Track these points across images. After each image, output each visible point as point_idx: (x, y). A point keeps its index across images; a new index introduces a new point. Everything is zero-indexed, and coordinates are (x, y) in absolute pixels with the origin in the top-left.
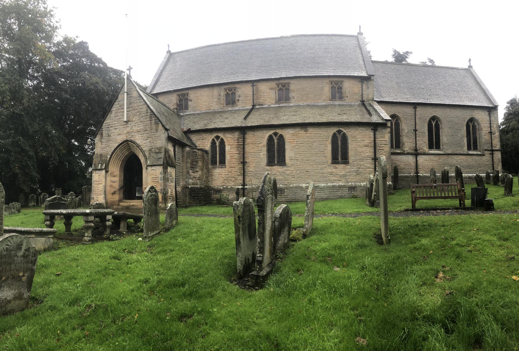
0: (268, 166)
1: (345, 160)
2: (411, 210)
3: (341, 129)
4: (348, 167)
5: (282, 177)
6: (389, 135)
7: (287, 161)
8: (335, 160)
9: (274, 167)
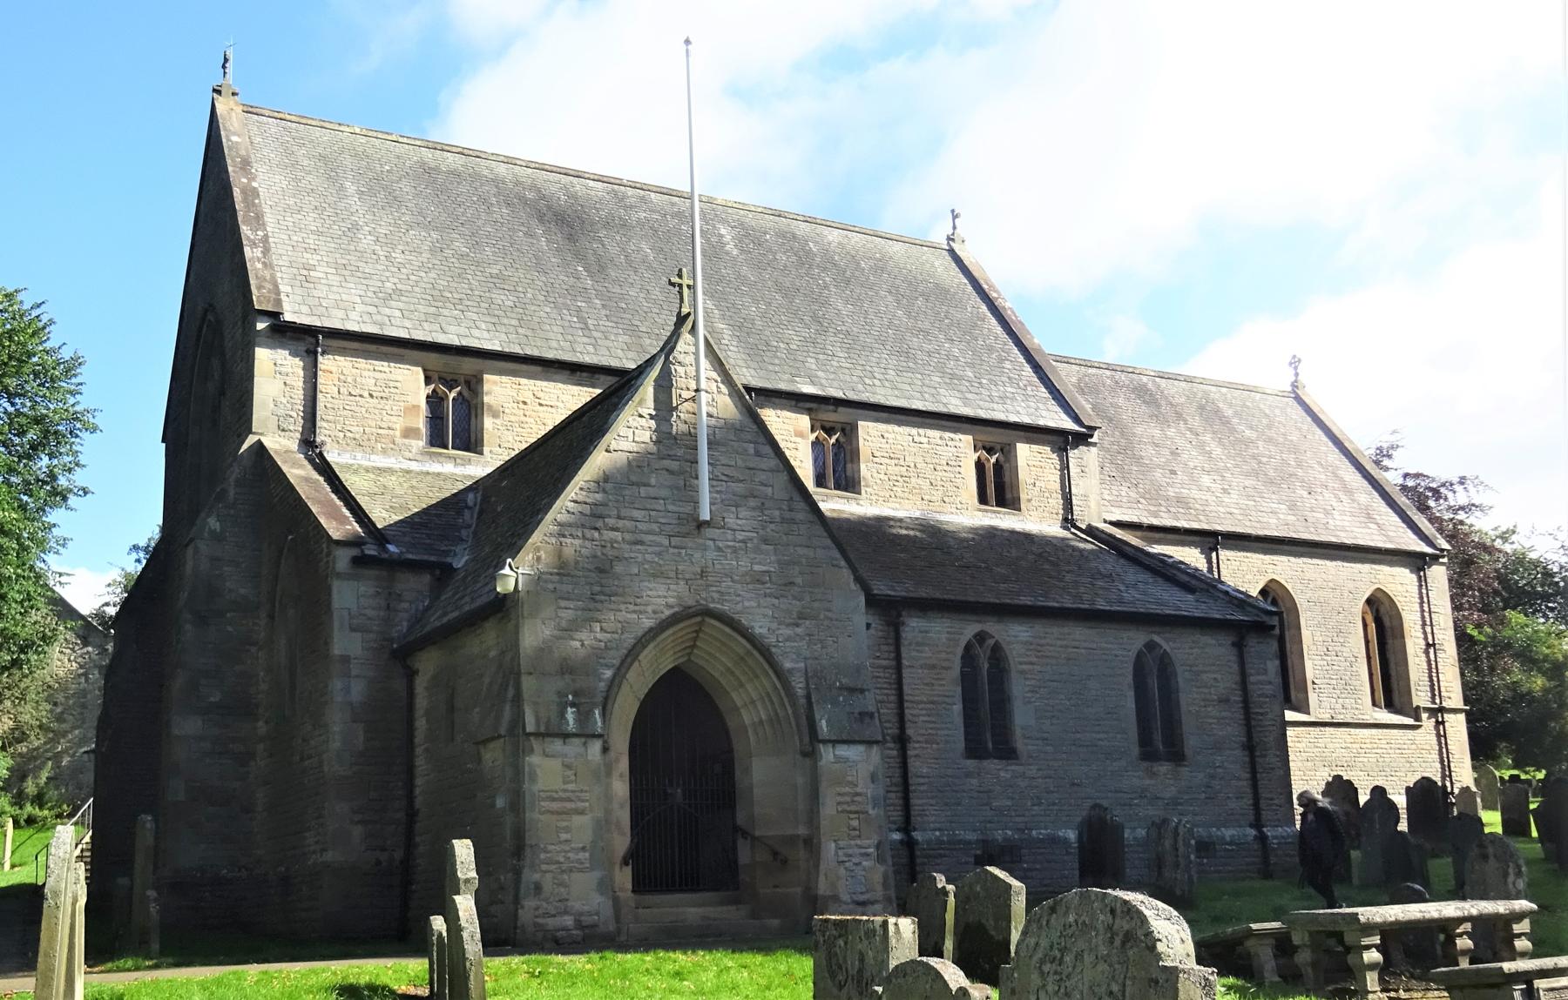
0: (968, 757)
1: (1176, 755)
2: (909, 844)
3: (1156, 638)
4: (1184, 771)
5: (1009, 803)
6: (1277, 662)
7: (1020, 744)
8: (1148, 754)
9: (985, 763)
